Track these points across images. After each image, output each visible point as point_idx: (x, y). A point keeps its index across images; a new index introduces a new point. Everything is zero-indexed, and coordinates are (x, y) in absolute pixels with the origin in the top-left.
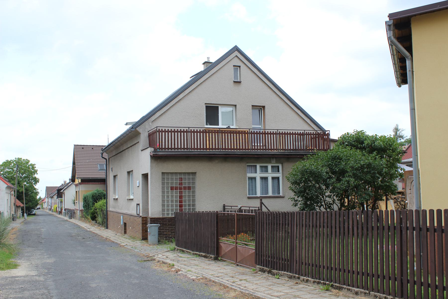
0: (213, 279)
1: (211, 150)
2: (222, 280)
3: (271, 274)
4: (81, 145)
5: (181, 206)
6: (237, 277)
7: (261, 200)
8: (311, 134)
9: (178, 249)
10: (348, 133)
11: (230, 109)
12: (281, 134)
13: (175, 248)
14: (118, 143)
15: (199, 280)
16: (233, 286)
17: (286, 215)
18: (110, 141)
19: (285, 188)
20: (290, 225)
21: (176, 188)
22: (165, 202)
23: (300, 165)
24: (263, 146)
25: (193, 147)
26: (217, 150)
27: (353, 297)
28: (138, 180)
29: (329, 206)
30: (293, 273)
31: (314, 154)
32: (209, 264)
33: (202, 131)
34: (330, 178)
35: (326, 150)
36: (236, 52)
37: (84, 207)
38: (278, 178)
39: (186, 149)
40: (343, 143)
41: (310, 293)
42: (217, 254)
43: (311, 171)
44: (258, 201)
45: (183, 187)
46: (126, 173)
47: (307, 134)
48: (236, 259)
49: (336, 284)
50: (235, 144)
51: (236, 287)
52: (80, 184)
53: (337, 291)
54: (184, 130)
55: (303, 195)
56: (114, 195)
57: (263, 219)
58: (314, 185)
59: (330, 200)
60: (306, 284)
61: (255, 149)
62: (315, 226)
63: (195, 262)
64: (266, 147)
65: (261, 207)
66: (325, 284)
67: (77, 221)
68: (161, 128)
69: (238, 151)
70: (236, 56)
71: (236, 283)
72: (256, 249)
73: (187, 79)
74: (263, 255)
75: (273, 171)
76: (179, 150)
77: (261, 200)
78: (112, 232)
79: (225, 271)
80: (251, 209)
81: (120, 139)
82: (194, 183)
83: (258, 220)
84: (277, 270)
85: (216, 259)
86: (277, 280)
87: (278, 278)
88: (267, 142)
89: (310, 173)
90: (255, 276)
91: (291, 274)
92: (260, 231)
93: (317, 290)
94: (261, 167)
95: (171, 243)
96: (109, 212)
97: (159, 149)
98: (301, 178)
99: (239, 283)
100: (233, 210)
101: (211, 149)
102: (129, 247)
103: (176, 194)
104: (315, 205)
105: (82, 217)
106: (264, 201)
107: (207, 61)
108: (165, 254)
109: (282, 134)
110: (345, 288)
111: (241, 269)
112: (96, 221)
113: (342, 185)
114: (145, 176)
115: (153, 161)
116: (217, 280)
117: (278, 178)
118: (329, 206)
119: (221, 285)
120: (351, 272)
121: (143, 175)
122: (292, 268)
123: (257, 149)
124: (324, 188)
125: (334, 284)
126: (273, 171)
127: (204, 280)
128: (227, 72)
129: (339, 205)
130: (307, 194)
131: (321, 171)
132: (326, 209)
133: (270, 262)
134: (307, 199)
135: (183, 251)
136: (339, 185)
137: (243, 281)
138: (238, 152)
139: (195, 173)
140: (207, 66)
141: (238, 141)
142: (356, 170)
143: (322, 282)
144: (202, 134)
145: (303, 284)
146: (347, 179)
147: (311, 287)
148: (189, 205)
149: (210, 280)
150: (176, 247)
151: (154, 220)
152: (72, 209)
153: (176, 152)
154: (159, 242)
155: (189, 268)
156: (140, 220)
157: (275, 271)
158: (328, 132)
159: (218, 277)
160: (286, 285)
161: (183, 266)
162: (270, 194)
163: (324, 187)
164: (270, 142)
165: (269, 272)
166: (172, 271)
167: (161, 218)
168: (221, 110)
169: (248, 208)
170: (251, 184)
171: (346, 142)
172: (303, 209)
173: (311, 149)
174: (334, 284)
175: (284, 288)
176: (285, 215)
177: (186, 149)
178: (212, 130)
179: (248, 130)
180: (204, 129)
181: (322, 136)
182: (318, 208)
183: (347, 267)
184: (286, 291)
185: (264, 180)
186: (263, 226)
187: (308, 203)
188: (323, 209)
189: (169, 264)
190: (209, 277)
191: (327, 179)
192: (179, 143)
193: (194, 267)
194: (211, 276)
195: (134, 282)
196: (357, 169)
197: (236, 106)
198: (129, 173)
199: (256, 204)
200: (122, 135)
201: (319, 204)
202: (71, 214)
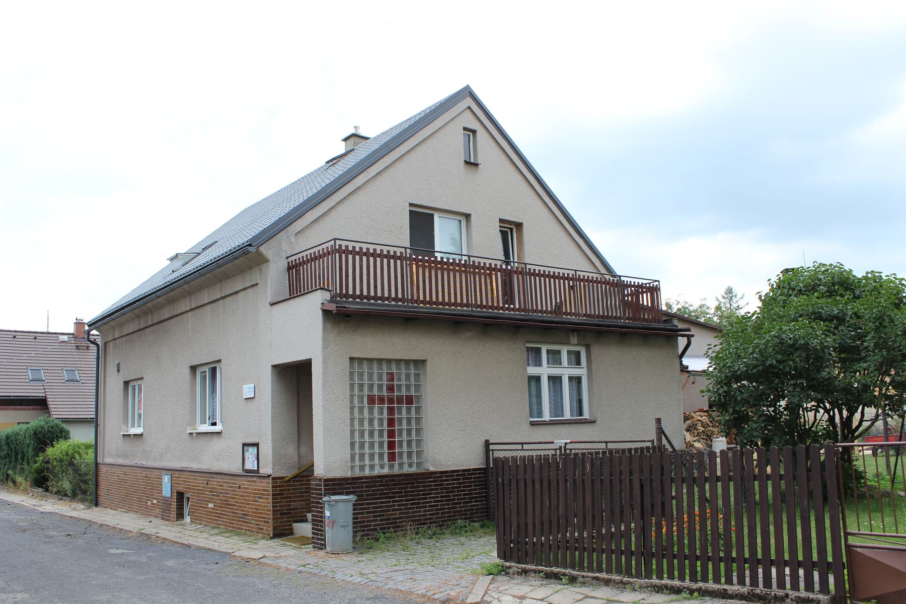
21: (381, 400)
46: (188, 370)
56: (124, 427)
65: (660, 440)
70: (469, 107)
96: (103, 470)
103: (380, 414)
107: (353, 131)
115: (328, 326)
121: (274, 366)
128: (453, 138)
139: (424, 362)
153: (380, 305)
167: (348, 479)
169: (603, 446)
197: (468, 216)
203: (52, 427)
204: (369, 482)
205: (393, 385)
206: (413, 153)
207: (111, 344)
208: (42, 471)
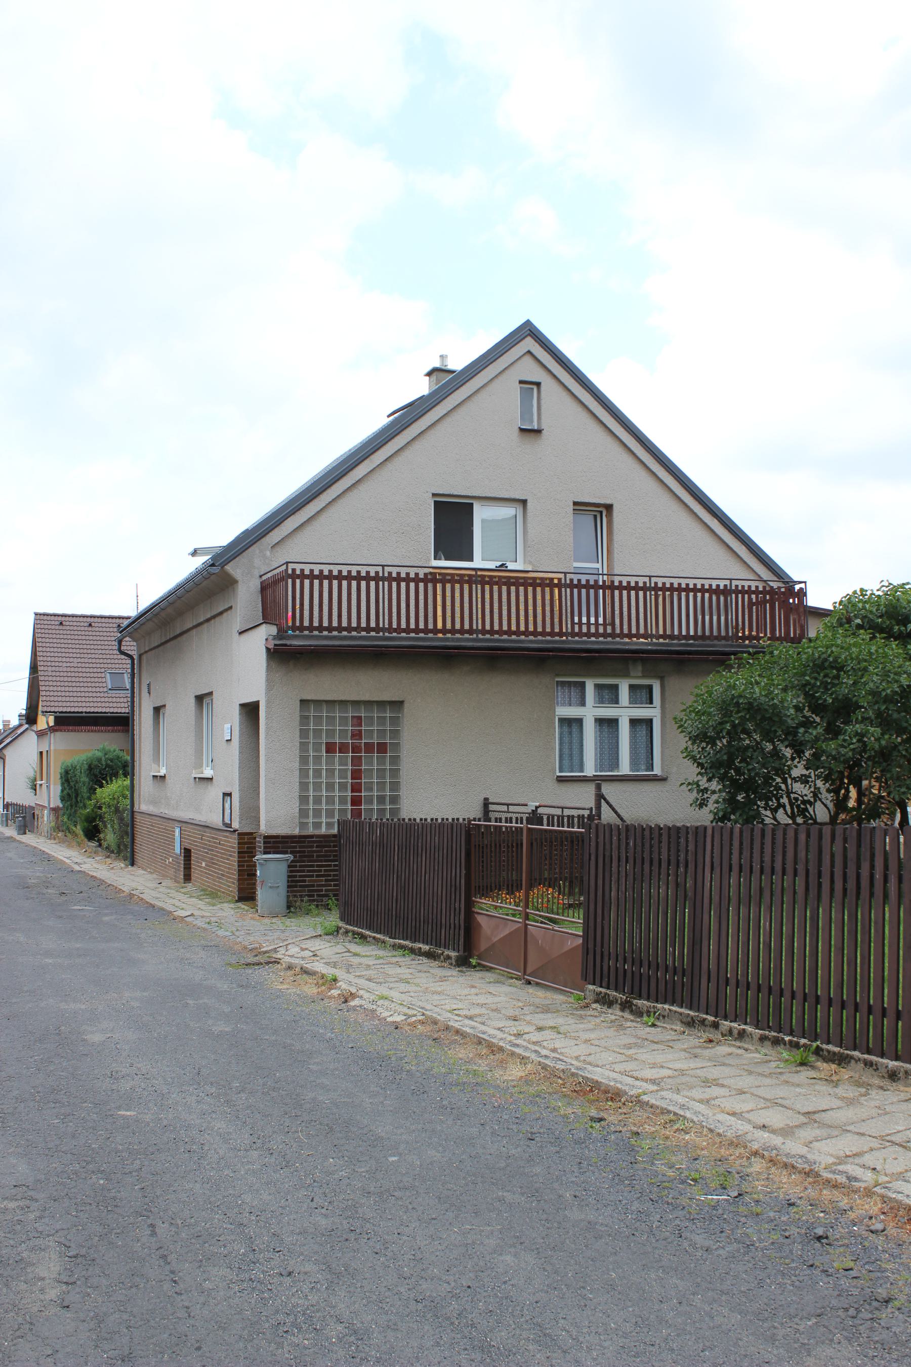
0: (456, 1025)
1: (449, 635)
2: (483, 1028)
3: (632, 1012)
4: (55, 615)
5: (356, 801)
6: (528, 1018)
7: (598, 787)
8: (749, 592)
9: (347, 932)
10: (862, 590)
11: (508, 511)
12: (660, 589)
13: (338, 929)
14: (170, 610)
15: (413, 1025)
16: (518, 1045)
17: (660, 835)
18: (144, 604)
19: (670, 752)
20: (691, 866)
21: (343, 748)
22: (308, 790)
23: (716, 684)
24: (605, 625)
25: (395, 626)
26: (467, 636)
27: (881, 1088)
28: (227, 723)
29: (801, 808)
30: (698, 1011)
31: (760, 651)
32: (443, 979)
33: (421, 576)
34: (807, 724)
35: (797, 640)
36: (529, 338)
37: (62, 799)
38: (649, 722)
39: (373, 630)
40: (849, 621)
41: (750, 1073)
42: (462, 946)
43: (750, 704)
44: (591, 789)
45: (362, 746)
46: (192, 701)
47: (737, 591)
48: (524, 964)
49: (830, 1047)
50: (522, 618)
51: (526, 1048)
52: (52, 729)
53: (834, 1066)
54: (330, 571)
55: (726, 773)
56: (154, 766)
57: (608, 847)
58: (758, 743)
59: (805, 791)
60: (738, 1044)
61: (580, 634)
62: (767, 869)
63: (399, 970)
64: (613, 628)
65: (598, 807)
66: (797, 1046)
67: (42, 840)
68: (298, 568)
69: (531, 638)
70: (529, 352)
71: (526, 1037)
72: (586, 937)
73: (380, 421)
74: (606, 953)
75: (633, 701)
76: (354, 633)
77: (598, 787)
78: (149, 876)
79: (490, 1000)
80: (567, 812)
81: (173, 597)
82: (395, 733)
83: (593, 851)
84: (648, 999)
85: (463, 962)
86: (648, 1029)
87: (654, 1025)
88: (617, 612)
89: (748, 710)
90: (581, 1017)
91: (692, 1013)
92: (600, 882)
93: (773, 1064)
94: (598, 687)
95: (325, 913)
96: (138, 817)
97: (294, 628)
98: (721, 723)
99: (536, 1036)
100: (514, 816)
101: (450, 631)
102: (200, 923)
103: (342, 764)
104: (761, 803)
105: (58, 828)
106: (606, 789)
107: (437, 364)
108: (309, 944)
109: (664, 589)
110: (858, 1060)
111: (538, 995)
112: (99, 841)
113: (843, 746)
114: (250, 711)
116: (467, 1026)
117: (649, 722)
118: (801, 808)
119: (480, 1041)
120: (877, 1010)
122: (696, 994)
123: (588, 635)
124: (789, 755)
125: (824, 1046)
126: (633, 701)
127: (429, 1028)
128: (502, 400)
129: (831, 806)
130: (738, 771)
131: (782, 702)
132: (793, 817)
133: (626, 974)
134: (735, 786)
135: (363, 937)
136: (833, 745)
137: (547, 1032)
138: (531, 642)
139: (402, 702)
140: (438, 381)
141: (531, 608)
142: (885, 702)
143: (787, 1038)
144: (421, 585)
145: (730, 1045)
146: (858, 727)
147: (754, 1054)
148: (381, 800)
149: (447, 1028)
150: (341, 924)
151: (275, 843)
152: (26, 803)
153: (345, 638)
154: (289, 907)
155: (383, 990)
156: (234, 840)
157: (641, 1003)
158: (803, 585)
159: (471, 1018)
160: (678, 1045)
161: (362, 982)
162: (625, 769)
163: (788, 752)
164: (505, 608)
165: (626, 1006)
166: (330, 997)
167: (295, 837)
168: (481, 513)
169: (558, 812)
170: (566, 739)
171: (856, 617)
172: (725, 818)
173: (750, 638)
174: (824, 1046)
175: (670, 1057)
176: (675, 833)
177: (373, 630)
178: (452, 575)
179: (562, 576)
180: (427, 570)
181: (782, 596)
182: (768, 813)
183: (865, 995)
184: (678, 1065)
185: (605, 728)
186: (607, 868)
187: (739, 798)
188: (781, 816)
189: (323, 977)
190: (443, 1016)
191: (797, 728)
192: (355, 613)
193: (399, 988)
194: (449, 1015)
195: (216, 1029)
196: (888, 700)
197: (524, 502)
198: (200, 699)
199: (581, 799)
200: (180, 587)
201: (773, 803)
202: (24, 818)
203: (111, 760)
204: (321, 842)
205: (360, 731)
206: (439, 427)
207: (144, 657)
208: (94, 820)
